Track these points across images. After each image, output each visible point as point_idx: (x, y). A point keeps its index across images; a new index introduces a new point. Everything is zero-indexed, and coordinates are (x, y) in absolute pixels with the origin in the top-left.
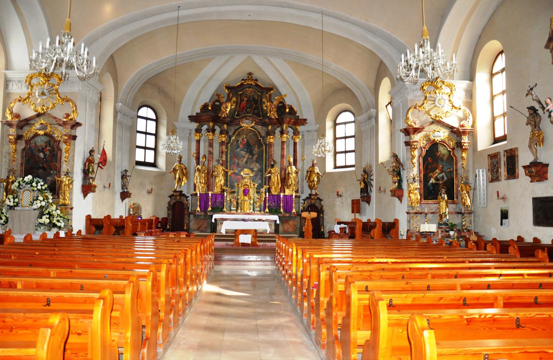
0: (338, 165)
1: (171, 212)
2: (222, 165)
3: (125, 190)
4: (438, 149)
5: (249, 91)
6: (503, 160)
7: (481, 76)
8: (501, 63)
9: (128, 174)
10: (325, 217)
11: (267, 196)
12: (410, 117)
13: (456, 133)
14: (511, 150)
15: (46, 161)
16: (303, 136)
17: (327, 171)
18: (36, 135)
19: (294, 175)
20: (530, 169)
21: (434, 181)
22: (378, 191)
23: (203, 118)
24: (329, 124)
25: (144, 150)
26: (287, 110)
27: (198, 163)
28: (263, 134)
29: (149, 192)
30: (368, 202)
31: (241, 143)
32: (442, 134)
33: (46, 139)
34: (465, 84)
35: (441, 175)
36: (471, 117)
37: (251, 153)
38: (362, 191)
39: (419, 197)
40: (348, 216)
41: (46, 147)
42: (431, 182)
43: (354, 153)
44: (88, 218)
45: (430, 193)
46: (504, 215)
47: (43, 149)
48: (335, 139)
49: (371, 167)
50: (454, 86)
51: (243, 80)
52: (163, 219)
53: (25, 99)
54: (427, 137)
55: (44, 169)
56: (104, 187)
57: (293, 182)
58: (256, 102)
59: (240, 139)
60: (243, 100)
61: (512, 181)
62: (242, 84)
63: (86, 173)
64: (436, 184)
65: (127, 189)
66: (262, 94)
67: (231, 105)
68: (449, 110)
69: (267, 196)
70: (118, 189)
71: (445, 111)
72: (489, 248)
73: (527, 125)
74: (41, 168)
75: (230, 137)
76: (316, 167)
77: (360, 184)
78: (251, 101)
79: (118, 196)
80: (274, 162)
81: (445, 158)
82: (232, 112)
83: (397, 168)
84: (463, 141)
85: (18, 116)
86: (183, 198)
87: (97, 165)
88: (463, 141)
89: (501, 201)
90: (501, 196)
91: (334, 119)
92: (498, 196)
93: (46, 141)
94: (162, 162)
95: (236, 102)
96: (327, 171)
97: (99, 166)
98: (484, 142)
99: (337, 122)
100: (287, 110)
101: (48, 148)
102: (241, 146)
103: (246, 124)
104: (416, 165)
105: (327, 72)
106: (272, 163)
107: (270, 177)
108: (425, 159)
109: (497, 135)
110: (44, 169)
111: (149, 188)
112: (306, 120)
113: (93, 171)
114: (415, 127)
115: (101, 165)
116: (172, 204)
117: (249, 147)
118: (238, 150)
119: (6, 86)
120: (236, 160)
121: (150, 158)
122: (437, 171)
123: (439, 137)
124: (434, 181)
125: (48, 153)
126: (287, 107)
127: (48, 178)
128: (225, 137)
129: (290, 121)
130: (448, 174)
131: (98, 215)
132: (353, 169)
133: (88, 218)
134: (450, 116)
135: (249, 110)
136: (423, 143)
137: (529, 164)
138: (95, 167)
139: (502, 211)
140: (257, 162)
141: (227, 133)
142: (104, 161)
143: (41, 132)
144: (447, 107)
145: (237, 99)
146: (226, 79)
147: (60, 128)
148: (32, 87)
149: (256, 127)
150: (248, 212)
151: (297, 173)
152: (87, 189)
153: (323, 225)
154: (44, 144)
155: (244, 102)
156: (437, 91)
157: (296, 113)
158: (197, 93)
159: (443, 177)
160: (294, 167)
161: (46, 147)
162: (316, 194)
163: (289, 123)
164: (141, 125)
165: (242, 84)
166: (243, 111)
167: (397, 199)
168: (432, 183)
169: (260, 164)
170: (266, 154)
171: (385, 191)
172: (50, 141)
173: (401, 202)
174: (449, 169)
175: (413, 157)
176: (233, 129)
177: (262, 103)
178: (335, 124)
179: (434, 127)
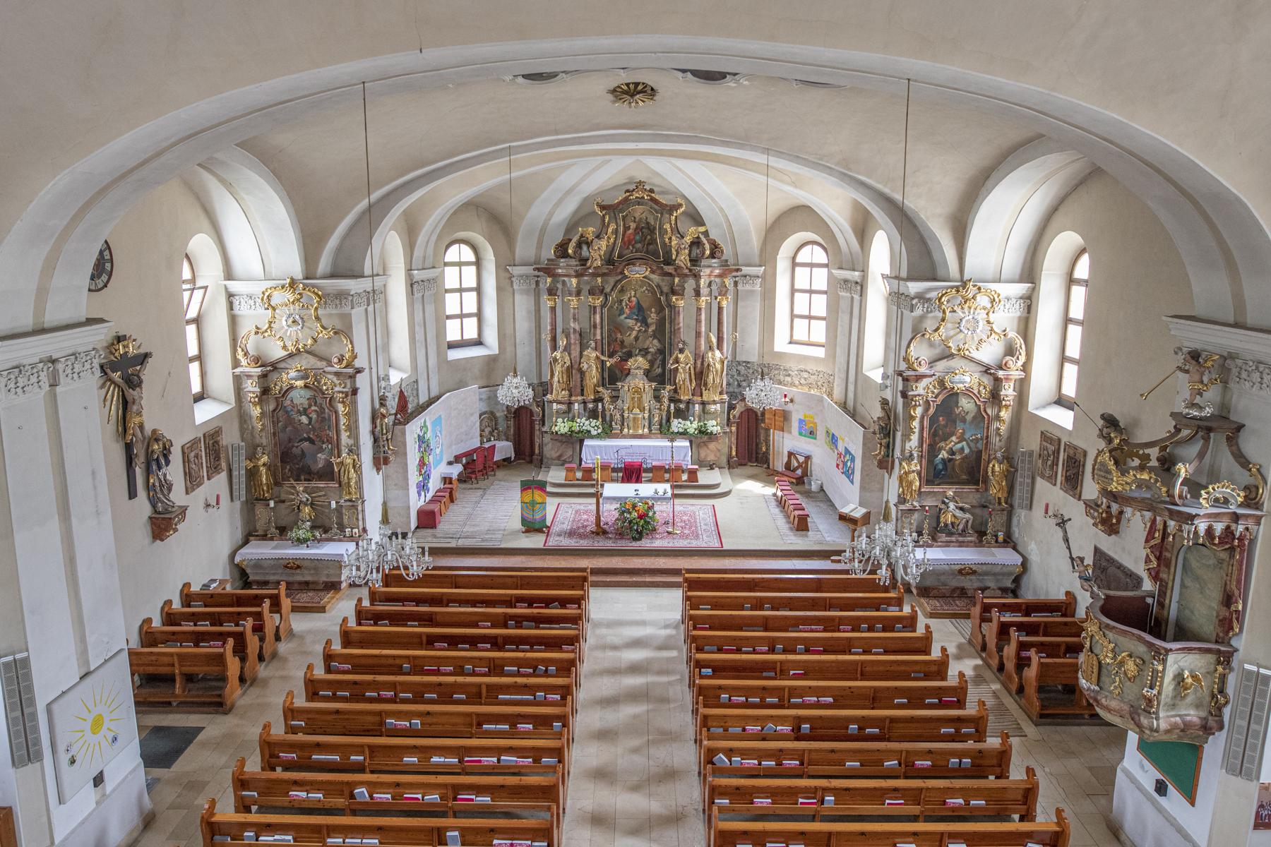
0: (795, 338)
5: (639, 212)
7: (1050, 284)
15: (314, 429)
18: (292, 387)
21: (946, 455)
24: (782, 265)
27: (554, 348)
28: (665, 289)
33: (308, 394)
35: (959, 446)
36: (1023, 353)
37: (644, 322)
41: (310, 406)
45: (937, 474)
47: (305, 410)
51: (627, 191)
60: (629, 228)
62: (626, 199)
64: (950, 460)
80: (684, 343)
85: (258, 361)
90: (1050, 513)
94: (491, 337)
102: (627, 311)
103: (638, 272)
104: (917, 430)
106: (681, 346)
108: (933, 420)
110: (312, 442)
118: (622, 317)
119: (231, 306)
120: (619, 336)
121: (471, 332)
122: (954, 438)
124: (946, 455)
125: (314, 416)
130: (972, 445)
135: (639, 245)
140: (654, 337)
141: (602, 291)
143: (300, 383)
148: (274, 309)
150: (640, 432)
159: (962, 449)
160: (718, 353)
161: (310, 406)
164: (451, 278)
175: (913, 418)
178: (794, 264)
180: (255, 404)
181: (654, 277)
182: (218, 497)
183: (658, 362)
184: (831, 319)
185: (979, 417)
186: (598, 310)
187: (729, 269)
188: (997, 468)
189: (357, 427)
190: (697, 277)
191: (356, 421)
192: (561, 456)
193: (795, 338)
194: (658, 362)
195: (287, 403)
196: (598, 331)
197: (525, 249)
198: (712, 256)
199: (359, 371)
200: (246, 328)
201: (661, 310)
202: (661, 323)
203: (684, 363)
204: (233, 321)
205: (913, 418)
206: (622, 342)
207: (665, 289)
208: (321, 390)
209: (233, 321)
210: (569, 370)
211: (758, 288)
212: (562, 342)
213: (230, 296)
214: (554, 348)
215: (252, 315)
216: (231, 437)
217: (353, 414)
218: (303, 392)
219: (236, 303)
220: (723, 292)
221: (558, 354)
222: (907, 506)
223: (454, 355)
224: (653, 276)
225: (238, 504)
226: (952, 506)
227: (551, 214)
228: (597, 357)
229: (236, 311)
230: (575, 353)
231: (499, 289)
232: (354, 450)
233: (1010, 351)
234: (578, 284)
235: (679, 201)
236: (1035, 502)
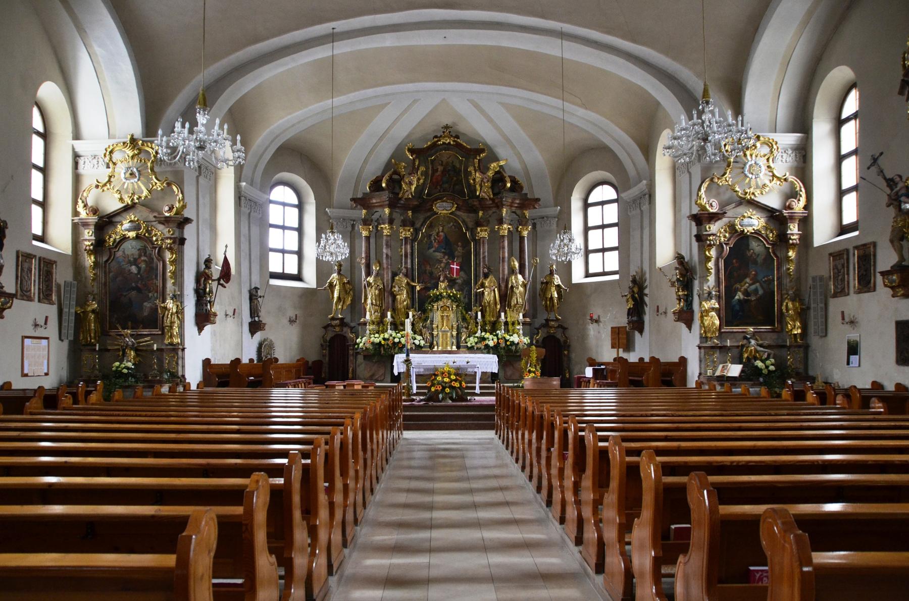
0: (591, 271)
1: (326, 352)
2: (406, 276)
3: (257, 319)
4: (748, 245)
5: (445, 155)
6: (854, 260)
7: (821, 129)
8: (852, 105)
9: (260, 293)
10: (573, 356)
12: (703, 196)
13: (777, 219)
14: (864, 245)
15: (142, 279)
16: (534, 226)
17: (574, 282)
18: (124, 238)
19: (521, 289)
20: (890, 277)
22: (655, 313)
23: (374, 201)
25: (281, 254)
26: (509, 185)
27: (368, 274)
28: (470, 225)
29: (292, 321)
30: (641, 331)
31: (435, 239)
32: (755, 222)
33: (137, 245)
34: (791, 139)
35: (753, 287)
36: (803, 194)
37: (452, 256)
38: (630, 313)
39: (717, 322)
40: (608, 354)
42: (737, 297)
43: (617, 252)
44: (206, 363)
45: (733, 314)
46: (853, 349)
47: (135, 260)
48: (587, 229)
49: (643, 274)
50: (776, 143)
51: (436, 137)
52: (314, 362)
53: (105, 185)
54: (732, 227)
55: (139, 290)
56: (226, 315)
57: (520, 300)
58: (457, 172)
61: (866, 296)
63: (201, 296)
64: (746, 301)
65: (258, 317)
67: (419, 179)
68: (767, 182)
70: (247, 319)
71: (760, 184)
72: (839, 400)
73: (888, 206)
74: (133, 289)
75: (417, 231)
76: (556, 276)
77: (627, 301)
79: (246, 328)
81: (760, 260)
82: (420, 190)
83: (686, 274)
84: (789, 232)
85: (95, 211)
86: (345, 329)
87: (216, 282)
88: (789, 232)
89: (847, 327)
90: (847, 319)
91: (583, 196)
92: (843, 319)
93: (139, 247)
95: (425, 174)
96: (574, 282)
97: (219, 284)
98: (823, 233)
99: (590, 201)
100: (509, 185)
101: (143, 258)
102: (436, 245)
103: (443, 208)
104: (713, 271)
105: (571, 121)
107: (483, 293)
109: (846, 221)
110: (139, 290)
111: (291, 313)
112: (538, 200)
113: (211, 291)
114: (711, 211)
115: (222, 282)
119: (76, 165)
120: (428, 268)
121: (292, 269)
122: (748, 280)
123: (751, 226)
125: (143, 266)
126: (508, 179)
127: (145, 304)
129: (512, 202)
130: (765, 285)
131: (223, 358)
132: (617, 277)
133: (206, 363)
134: (770, 191)
135: (446, 186)
136: (725, 237)
137: (889, 269)
138: (215, 284)
139: (849, 343)
141: (412, 224)
142: (226, 274)
143: (132, 234)
144: (764, 177)
145: (427, 168)
146: (408, 136)
147: (161, 227)
150: (449, 348)
151: (524, 285)
152: (203, 318)
153: (569, 368)
154: (136, 252)
155: (439, 173)
156: (748, 153)
157: (521, 188)
158: (361, 155)
159: (756, 290)
160: (520, 277)
161: (140, 256)
162: (557, 320)
163: (511, 206)
164: (275, 214)
165: (434, 145)
166: (436, 188)
167: (683, 326)
168: (739, 300)
169: (465, 272)
170: (476, 256)
171: (665, 313)
172: (145, 247)
173: (690, 330)
174: (767, 276)
175: (708, 259)
176: (421, 217)
177: (468, 174)
178: (586, 206)
179: (741, 210)
180: (90, 252)
182: (47, 317)
184: (623, 225)
185: (768, 260)
186: (409, 241)
187: (529, 202)
188: (790, 305)
189: (182, 276)
191: (182, 270)
192: (373, 375)
193: (591, 271)
195: (119, 254)
197: (342, 193)
199: (187, 221)
200: (87, 182)
204: (77, 179)
205: (708, 259)
207: (470, 225)
208: (152, 242)
209: (77, 179)
210: (382, 291)
212: (375, 268)
213: (76, 156)
214: (368, 274)
215: (92, 172)
216: (63, 275)
217: (179, 262)
218: (134, 243)
219: (81, 161)
221: (371, 279)
222: (709, 344)
223: (274, 282)
224: (458, 213)
225: (66, 344)
226: (753, 342)
227: (366, 161)
228: (408, 284)
229: (81, 170)
230: (388, 276)
232: (178, 298)
233: (793, 194)
234: (390, 214)
236: (829, 330)
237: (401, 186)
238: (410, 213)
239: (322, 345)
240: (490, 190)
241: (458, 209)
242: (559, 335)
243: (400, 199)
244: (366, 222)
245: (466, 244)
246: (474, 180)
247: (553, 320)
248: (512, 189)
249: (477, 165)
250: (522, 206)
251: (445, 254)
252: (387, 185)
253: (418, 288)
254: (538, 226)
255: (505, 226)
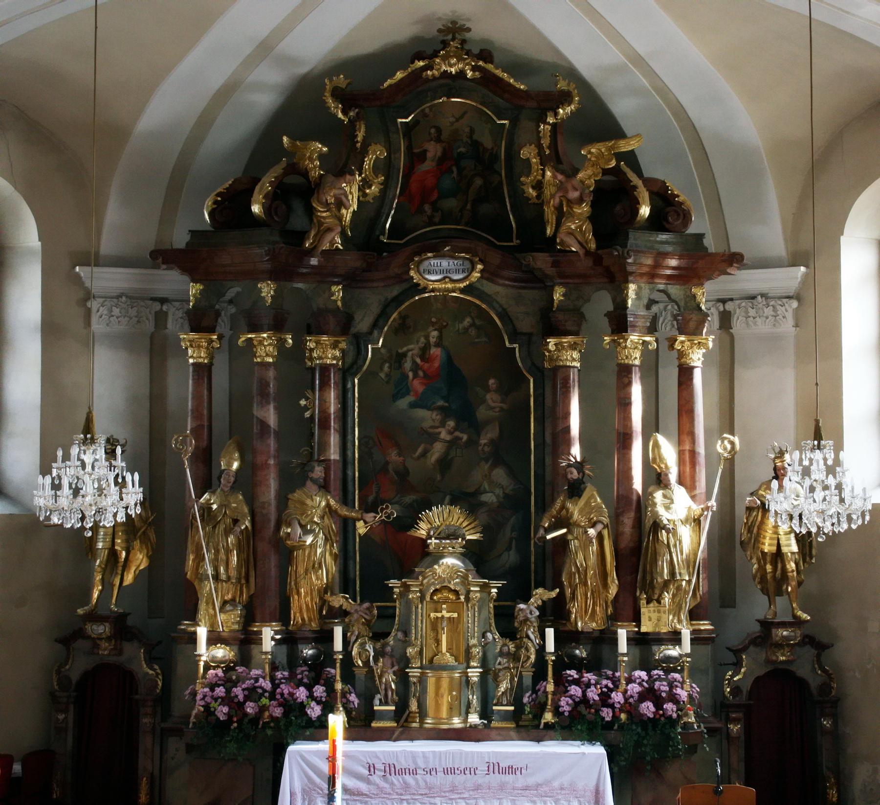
1: (67, 718)
2: (324, 487)
11: (550, 646)
26: (645, 211)
28: (526, 323)
31: (415, 368)
37: (465, 415)
58: (484, 160)
59: (413, 349)
66: (514, 122)
67: (366, 184)
69: (550, 646)
75: (359, 342)
78: (461, 156)
95: (386, 167)
100: (645, 211)
102: (418, 386)
103: (440, 274)
107: (562, 543)
116: (75, 676)
117: (454, 389)
118: (403, 403)
120: (394, 456)
126: (644, 194)
128: (335, 346)
135: (451, 204)
140: (497, 457)
145: (391, 149)
149: (489, 288)
150: (457, 722)
155: (428, 165)
160: (680, 493)
162: (797, 623)
176: (373, 300)
177: (516, 167)
181: (498, 290)
183: (508, 533)
187: (704, 262)
190: (616, 280)
194: (508, 533)
196: (334, 439)
198: (657, 223)
201: (513, 381)
202: (515, 420)
203: (587, 534)
206: (403, 474)
211: (787, 326)
214: (205, 484)
220: (689, 321)
224: (489, 288)
231: (51, 330)
235: (562, 85)
237: (310, 211)
238: (338, 292)
239: (53, 697)
240: (587, 226)
241: (488, 274)
242: (804, 670)
243: (310, 252)
244: (200, 321)
245: (513, 381)
246: (539, 186)
247: (784, 625)
248: (657, 223)
249: (546, 142)
250: (690, 275)
251: (446, 412)
252: (267, 209)
253: (361, 529)
254: (738, 326)
255: (634, 337)
